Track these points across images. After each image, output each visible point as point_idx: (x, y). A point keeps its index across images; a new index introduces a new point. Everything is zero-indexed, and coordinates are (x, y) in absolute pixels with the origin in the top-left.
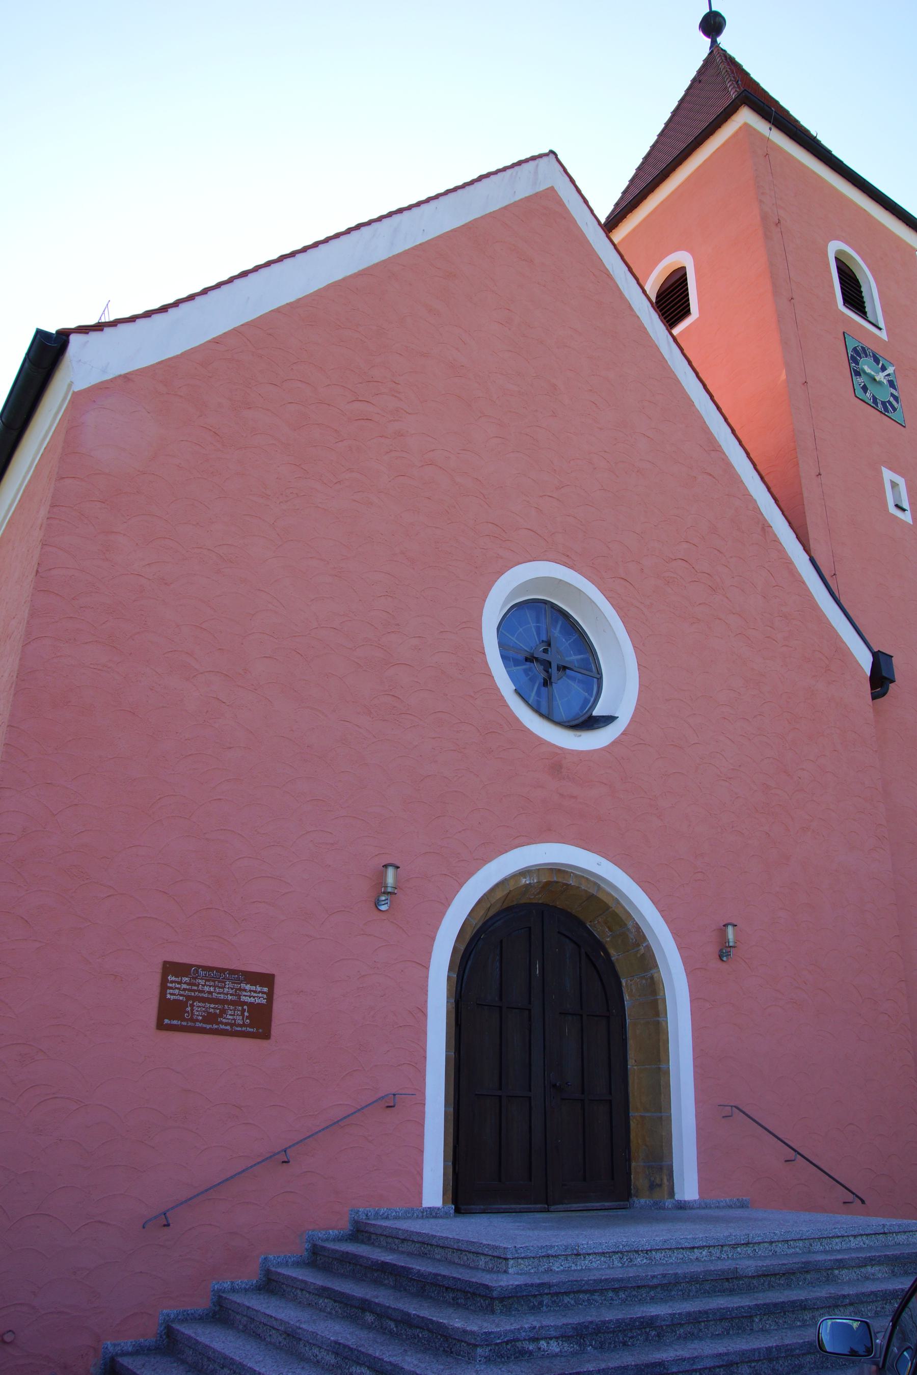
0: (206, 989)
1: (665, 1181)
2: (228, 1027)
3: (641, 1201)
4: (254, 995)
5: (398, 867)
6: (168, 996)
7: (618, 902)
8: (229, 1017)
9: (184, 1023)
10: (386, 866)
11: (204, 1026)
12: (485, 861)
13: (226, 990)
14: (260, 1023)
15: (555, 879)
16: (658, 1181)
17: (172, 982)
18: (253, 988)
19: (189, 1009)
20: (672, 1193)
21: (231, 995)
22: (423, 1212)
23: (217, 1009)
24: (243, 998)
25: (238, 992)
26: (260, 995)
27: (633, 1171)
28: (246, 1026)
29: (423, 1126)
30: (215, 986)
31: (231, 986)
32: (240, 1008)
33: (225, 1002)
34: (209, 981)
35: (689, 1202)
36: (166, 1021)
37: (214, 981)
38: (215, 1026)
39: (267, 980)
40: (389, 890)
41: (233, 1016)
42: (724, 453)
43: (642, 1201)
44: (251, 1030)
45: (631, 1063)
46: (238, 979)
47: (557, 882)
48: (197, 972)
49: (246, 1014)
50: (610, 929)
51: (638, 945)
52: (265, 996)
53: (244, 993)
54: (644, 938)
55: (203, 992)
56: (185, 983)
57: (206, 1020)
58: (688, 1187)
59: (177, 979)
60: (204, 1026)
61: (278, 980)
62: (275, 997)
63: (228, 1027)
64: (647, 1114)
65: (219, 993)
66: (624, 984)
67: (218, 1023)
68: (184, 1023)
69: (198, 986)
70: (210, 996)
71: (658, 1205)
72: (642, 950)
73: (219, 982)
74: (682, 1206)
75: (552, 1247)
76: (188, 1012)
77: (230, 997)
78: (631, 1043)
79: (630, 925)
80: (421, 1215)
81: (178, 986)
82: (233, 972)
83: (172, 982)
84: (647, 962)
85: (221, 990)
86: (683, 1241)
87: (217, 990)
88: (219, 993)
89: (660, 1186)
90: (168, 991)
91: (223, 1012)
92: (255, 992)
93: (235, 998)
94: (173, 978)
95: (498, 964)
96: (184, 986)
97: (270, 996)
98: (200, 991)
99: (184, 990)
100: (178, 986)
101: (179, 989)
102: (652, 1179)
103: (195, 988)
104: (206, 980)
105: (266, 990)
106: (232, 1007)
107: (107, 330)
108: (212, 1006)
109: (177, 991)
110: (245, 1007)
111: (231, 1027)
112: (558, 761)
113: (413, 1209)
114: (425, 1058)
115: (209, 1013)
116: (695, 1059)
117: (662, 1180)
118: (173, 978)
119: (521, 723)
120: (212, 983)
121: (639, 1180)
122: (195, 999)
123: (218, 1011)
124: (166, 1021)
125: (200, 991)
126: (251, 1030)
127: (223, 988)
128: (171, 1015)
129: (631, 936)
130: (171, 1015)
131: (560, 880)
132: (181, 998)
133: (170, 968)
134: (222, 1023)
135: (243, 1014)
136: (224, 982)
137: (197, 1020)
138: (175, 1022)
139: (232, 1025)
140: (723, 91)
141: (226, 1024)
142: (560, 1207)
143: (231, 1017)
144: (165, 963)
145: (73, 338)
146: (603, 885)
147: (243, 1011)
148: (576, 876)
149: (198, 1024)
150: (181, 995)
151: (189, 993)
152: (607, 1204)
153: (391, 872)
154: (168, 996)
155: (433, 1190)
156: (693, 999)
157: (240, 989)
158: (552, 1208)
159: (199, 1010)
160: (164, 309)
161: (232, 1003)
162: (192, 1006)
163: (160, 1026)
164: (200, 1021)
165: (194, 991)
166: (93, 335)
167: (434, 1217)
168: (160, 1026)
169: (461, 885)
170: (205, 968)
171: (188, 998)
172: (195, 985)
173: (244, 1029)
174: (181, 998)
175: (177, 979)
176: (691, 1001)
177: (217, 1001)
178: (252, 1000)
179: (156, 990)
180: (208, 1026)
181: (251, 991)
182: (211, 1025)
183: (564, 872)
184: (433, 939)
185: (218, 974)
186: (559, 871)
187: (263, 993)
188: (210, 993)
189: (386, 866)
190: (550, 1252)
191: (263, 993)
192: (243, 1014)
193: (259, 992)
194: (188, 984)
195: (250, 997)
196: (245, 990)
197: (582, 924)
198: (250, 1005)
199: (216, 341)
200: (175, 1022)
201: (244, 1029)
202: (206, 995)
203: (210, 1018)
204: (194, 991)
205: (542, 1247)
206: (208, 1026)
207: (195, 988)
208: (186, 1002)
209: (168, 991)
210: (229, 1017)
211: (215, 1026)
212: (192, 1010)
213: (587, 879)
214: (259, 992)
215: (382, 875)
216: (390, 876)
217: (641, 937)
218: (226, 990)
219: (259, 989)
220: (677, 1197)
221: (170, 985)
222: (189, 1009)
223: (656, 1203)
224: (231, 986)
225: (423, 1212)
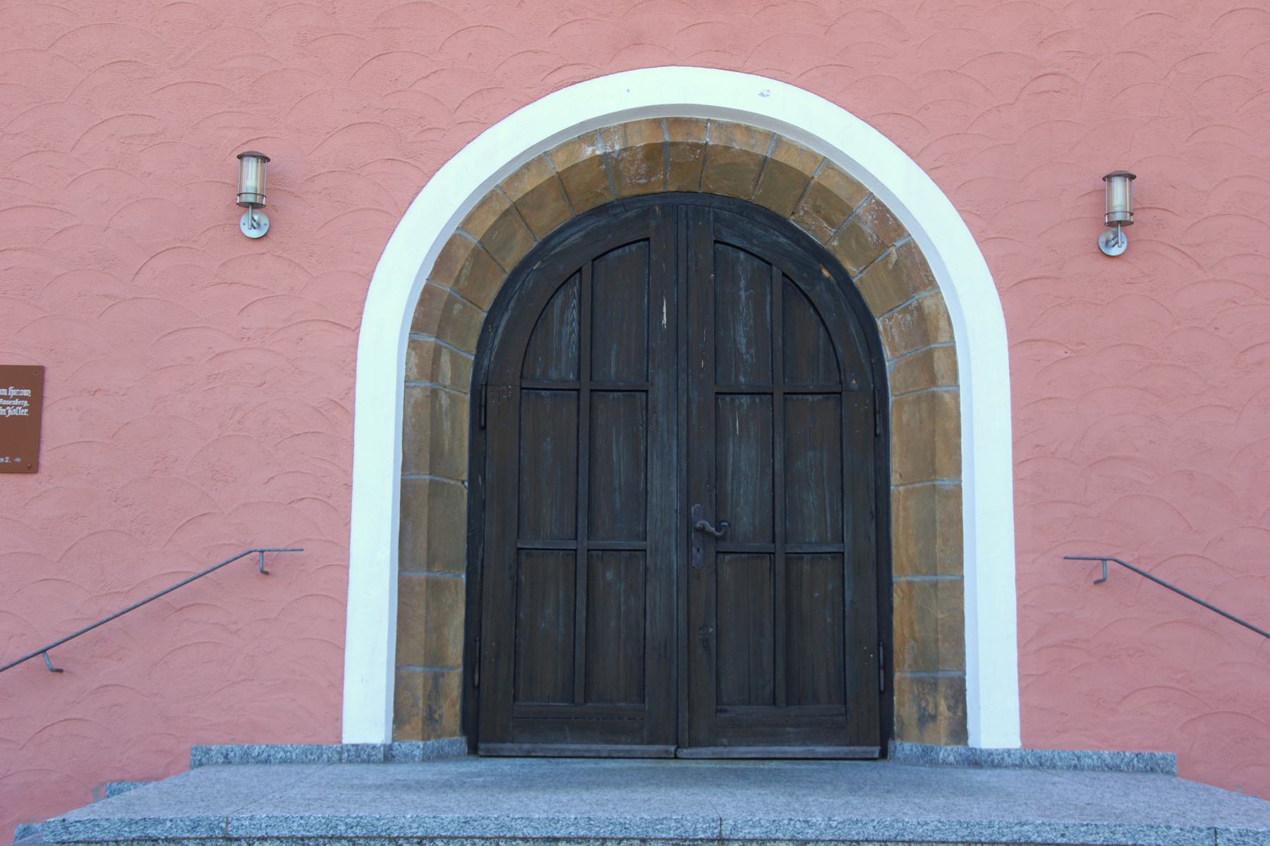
1: (943, 707)
3: (904, 747)
5: (1132, 177)
7: (827, 164)
10: (1108, 178)
12: (484, 124)
15: (667, 138)
16: (931, 710)
20: (960, 732)
22: (340, 753)
26: (16, 402)
27: (896, 688)
29: (343, 605)
35: (990, 753)
40: (1119, 217)
43: (907, 746)
45: (895, 478)
47: (674, 144)
50: (832, 224)
51: (884, 246)
54: (899, 230)
58: (996, 719)
64: (918, 579)
66: (881, 328)
71: (928, 758)
74: (978, 760)
75: (157, 822)
78: (895, 441)
79: (860, 207)
80: (336, 757)
84: (914, 273)
86: (519, 825)
89: (934, 718)
95: (575, 312)
97: (36, 403)
102: (923, 704)
105: (27, 393)
113: (319, 747)
114: (349, 486)
116: (1019, 464)
117: (936, 707)
121: (904, 707)
129: (867, 229)
131: (679, 139)
142: (704, 751)
146: (787, 136)
148: (720, 126)
152: (821, 750)
153: (1118, 186)
155: (366, 713)
156: (1018, 342)
158: (684, 752)
167: (363, 761)
176: (1012, 348)
183: (689, 122)
184: (368, 278)
186: (676, 122)
189: (1108, 178)
190: (152, 832)
193: (15, 398)
197: (780, 223)
205: (131, 822)
213: (748, 128)
215: (1104, 195)
216: (1119, 194)
220: (972, 742)
223: (925, 751)
225: (340, 753)
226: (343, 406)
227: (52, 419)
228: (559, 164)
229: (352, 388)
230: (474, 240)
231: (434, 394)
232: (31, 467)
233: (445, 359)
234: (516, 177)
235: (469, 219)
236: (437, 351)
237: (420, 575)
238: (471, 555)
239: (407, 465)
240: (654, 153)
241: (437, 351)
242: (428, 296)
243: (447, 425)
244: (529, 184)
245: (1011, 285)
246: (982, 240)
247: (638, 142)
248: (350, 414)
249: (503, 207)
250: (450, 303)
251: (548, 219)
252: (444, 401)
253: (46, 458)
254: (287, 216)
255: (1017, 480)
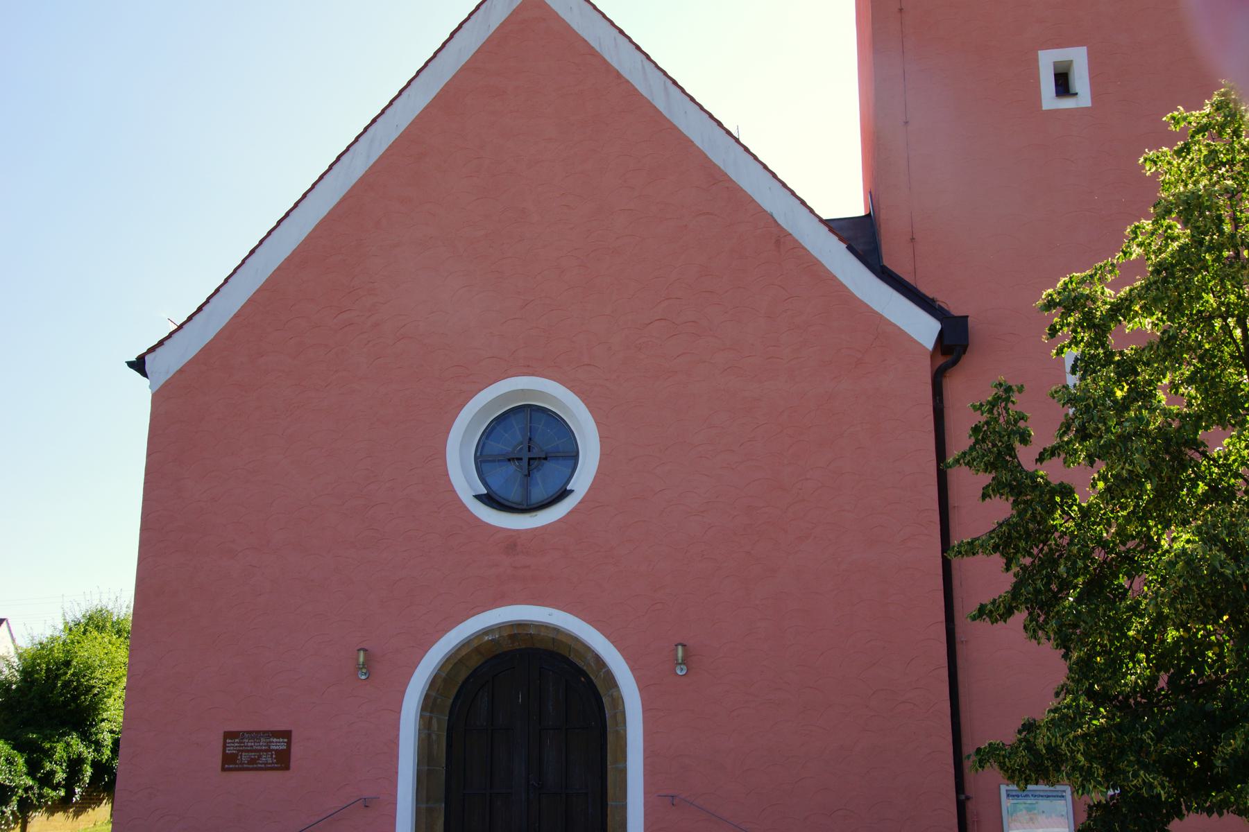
14: (283, 761)
25: (268, 744)
29: (394, 818)
39: (287, 734)
41: (266, 758)
42: (731, 180)
61: (294, 735)
79: (589, 656)
82: (264, 732)
91: (260, 757)
97: (289, 744)
107: (166, 343)
112: (512, 541)
114: (397, 773)
119: (479, 520)
128: (230, 762)
130: (230, 762)
133: (229, 735)
140: (139, 365)
145: (147, 358)
156: (646, 710)
159: (245, 757)
160: (200, 309)
163: (223, 769)
166: (159, 350)
168: (223, 769)
169: (426, 652)
170: (248, 732)
179: (221, 749)
182: (253, 765)
184: (404, 692)
185: (255, 735)
199: (236, 316)
203: (252, 761)
217: (433, 683)
226: (394, 742)
227: (295, 750)
228: (475, 644)
229: (398, 735)
230: (444, 675)
231: (429, 735)
232: (287, 768)
233: (434, 721)
234: (459, 649)
235: (442, 666)
236: (431, 718)
237: (424, 806)
238: (447, 798)
239: (419, 763)
240: (512, 637)
241: (431, 718)
242: (427, 697)
243: (435, 747)
244: (463, 653)
245: (644, 688)
246: (633, 669)
247: (505, 634)
248: (397, 745)
249: (454, 661)
250: (435, 699)
251: (475, 662)
252: (434, 737)
253: (292, 764)
254: (379, 670)
255: (645, 765)
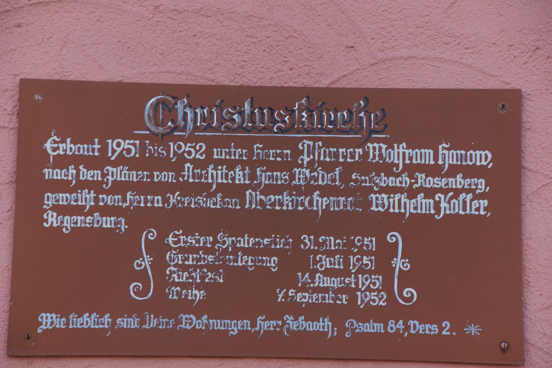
0: (216, 176)
2: (324, 325)
4: (439, 185)
6: (52, 219)
8: (321, 281)
9: (128, 323)
11: (218, 325)
13: (302, 175)
17: (62, 162)
18: (426, 156)
19: (145, 262)
21: (326, 191)
23: (268, 252)
24: (379, 203)
25: (354, 179)
26: (459, 181)
28: (405, 314)
30: (251, 164)
31: (323, 155)
32: (370, 242)
33: (305, 221)
34: (223, 143)
36: (48, 320)
37: (247, 144)
38: (264, 324)
39: (488, 119)
44: (431, 329)
46: (352, 125)
48: (171, 110)
49: (400, 263)
52: (481, 185)
53: (384, 181)
55: (202, 189)
56: (121, 161)
57: (217, 303)
59: (83, 149)
60: (218, 325)
62: (531, 184)
63: (324, 325)
65: (268, 190)
67: (276, 312)
68: (128, 323)
69: (178, 167)
70: (233, 204)
72: (11, 303)
73: (269, 144)
76: (142, 276)
77: (321, 203)
81: (87, 174)
83: (62, 162)
85: (281, 177)
87: (264, 177)
88: (268, 190)
90: (50, 199)
91: (297, 262)
92: (434, 171)
93: (341, 203)
94: (68, 147)
96: (118, 174)
97: (506, 183)
98: (187, 189)
99: (119, 188)
100: (87, 174)
101: (96, 186)
103: (168, 177)
104: (211, 143)
105: (481, 157)
106: (332, 242)
108: (246, 242)
109: (87, 198)
110: (394, 237)
111: (337, 322)
115: (233, 273)
118: (68, 147)
120: (238, 153)
122: (167, 220)
123: (272, 262)
124: (48, 320)
125: (187, 189)
126: (431, 329)
127: (287, 166)
132: (108, 222)
134: (296, 309)
135: (384, 267)
136: (293, 144)
137: (185, 306)
138: (87, 321)
139: (337, 314)
141: (313, 312)
143: (334, 283)
144: (27, 87)
147: (385, 253)
149: (189, 322)
150: (106, 211)
151: (141, 201)
154: (52, 219)
157: (365, 166)
161: (331, 222)
162: (158, 249)
164: (198, 310)
165: (163, 189)
170: (198, 95)
171: (138, 218)
172: (164, 164)
173: (393, 326)
174: (108, 222)
175: (83, 149)
177: (264, 222)
178: (423, 205)
180: (235, 327)
181: (411, 169)
187: (471, 172)
188: (232, 190)
191: (471, 172)
192: (384, 267)
193: (453, 171)
194: (133, 164)
195: (412, 193)
196: (388, 169)
198: (416, 227)
200: (87, 321)
201: (393, 326)
202: (215, 203)
203: (239, 292)
204: (163, 189)
206: (235, 327)
207: (168, 177)
208: (127, 245)
209: (50, 199)
210: (321, 281)
211: (264, 324)
212: (160, 265)
214: (453, 171)
218: (302, 175)
219: (448, 156)
221: (57, 174)
222: (145, 262)
224: (323, 155)
